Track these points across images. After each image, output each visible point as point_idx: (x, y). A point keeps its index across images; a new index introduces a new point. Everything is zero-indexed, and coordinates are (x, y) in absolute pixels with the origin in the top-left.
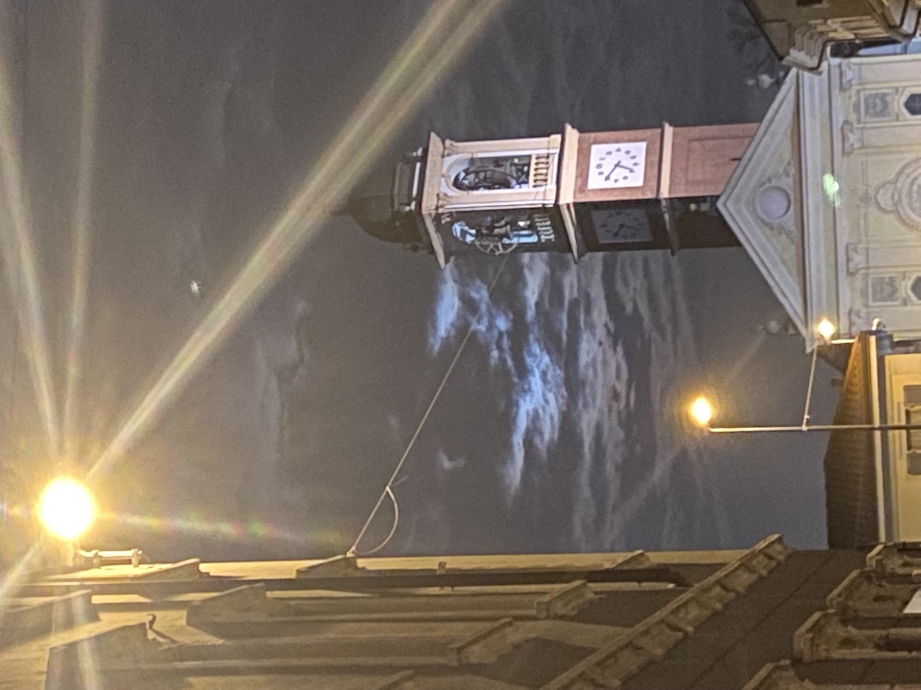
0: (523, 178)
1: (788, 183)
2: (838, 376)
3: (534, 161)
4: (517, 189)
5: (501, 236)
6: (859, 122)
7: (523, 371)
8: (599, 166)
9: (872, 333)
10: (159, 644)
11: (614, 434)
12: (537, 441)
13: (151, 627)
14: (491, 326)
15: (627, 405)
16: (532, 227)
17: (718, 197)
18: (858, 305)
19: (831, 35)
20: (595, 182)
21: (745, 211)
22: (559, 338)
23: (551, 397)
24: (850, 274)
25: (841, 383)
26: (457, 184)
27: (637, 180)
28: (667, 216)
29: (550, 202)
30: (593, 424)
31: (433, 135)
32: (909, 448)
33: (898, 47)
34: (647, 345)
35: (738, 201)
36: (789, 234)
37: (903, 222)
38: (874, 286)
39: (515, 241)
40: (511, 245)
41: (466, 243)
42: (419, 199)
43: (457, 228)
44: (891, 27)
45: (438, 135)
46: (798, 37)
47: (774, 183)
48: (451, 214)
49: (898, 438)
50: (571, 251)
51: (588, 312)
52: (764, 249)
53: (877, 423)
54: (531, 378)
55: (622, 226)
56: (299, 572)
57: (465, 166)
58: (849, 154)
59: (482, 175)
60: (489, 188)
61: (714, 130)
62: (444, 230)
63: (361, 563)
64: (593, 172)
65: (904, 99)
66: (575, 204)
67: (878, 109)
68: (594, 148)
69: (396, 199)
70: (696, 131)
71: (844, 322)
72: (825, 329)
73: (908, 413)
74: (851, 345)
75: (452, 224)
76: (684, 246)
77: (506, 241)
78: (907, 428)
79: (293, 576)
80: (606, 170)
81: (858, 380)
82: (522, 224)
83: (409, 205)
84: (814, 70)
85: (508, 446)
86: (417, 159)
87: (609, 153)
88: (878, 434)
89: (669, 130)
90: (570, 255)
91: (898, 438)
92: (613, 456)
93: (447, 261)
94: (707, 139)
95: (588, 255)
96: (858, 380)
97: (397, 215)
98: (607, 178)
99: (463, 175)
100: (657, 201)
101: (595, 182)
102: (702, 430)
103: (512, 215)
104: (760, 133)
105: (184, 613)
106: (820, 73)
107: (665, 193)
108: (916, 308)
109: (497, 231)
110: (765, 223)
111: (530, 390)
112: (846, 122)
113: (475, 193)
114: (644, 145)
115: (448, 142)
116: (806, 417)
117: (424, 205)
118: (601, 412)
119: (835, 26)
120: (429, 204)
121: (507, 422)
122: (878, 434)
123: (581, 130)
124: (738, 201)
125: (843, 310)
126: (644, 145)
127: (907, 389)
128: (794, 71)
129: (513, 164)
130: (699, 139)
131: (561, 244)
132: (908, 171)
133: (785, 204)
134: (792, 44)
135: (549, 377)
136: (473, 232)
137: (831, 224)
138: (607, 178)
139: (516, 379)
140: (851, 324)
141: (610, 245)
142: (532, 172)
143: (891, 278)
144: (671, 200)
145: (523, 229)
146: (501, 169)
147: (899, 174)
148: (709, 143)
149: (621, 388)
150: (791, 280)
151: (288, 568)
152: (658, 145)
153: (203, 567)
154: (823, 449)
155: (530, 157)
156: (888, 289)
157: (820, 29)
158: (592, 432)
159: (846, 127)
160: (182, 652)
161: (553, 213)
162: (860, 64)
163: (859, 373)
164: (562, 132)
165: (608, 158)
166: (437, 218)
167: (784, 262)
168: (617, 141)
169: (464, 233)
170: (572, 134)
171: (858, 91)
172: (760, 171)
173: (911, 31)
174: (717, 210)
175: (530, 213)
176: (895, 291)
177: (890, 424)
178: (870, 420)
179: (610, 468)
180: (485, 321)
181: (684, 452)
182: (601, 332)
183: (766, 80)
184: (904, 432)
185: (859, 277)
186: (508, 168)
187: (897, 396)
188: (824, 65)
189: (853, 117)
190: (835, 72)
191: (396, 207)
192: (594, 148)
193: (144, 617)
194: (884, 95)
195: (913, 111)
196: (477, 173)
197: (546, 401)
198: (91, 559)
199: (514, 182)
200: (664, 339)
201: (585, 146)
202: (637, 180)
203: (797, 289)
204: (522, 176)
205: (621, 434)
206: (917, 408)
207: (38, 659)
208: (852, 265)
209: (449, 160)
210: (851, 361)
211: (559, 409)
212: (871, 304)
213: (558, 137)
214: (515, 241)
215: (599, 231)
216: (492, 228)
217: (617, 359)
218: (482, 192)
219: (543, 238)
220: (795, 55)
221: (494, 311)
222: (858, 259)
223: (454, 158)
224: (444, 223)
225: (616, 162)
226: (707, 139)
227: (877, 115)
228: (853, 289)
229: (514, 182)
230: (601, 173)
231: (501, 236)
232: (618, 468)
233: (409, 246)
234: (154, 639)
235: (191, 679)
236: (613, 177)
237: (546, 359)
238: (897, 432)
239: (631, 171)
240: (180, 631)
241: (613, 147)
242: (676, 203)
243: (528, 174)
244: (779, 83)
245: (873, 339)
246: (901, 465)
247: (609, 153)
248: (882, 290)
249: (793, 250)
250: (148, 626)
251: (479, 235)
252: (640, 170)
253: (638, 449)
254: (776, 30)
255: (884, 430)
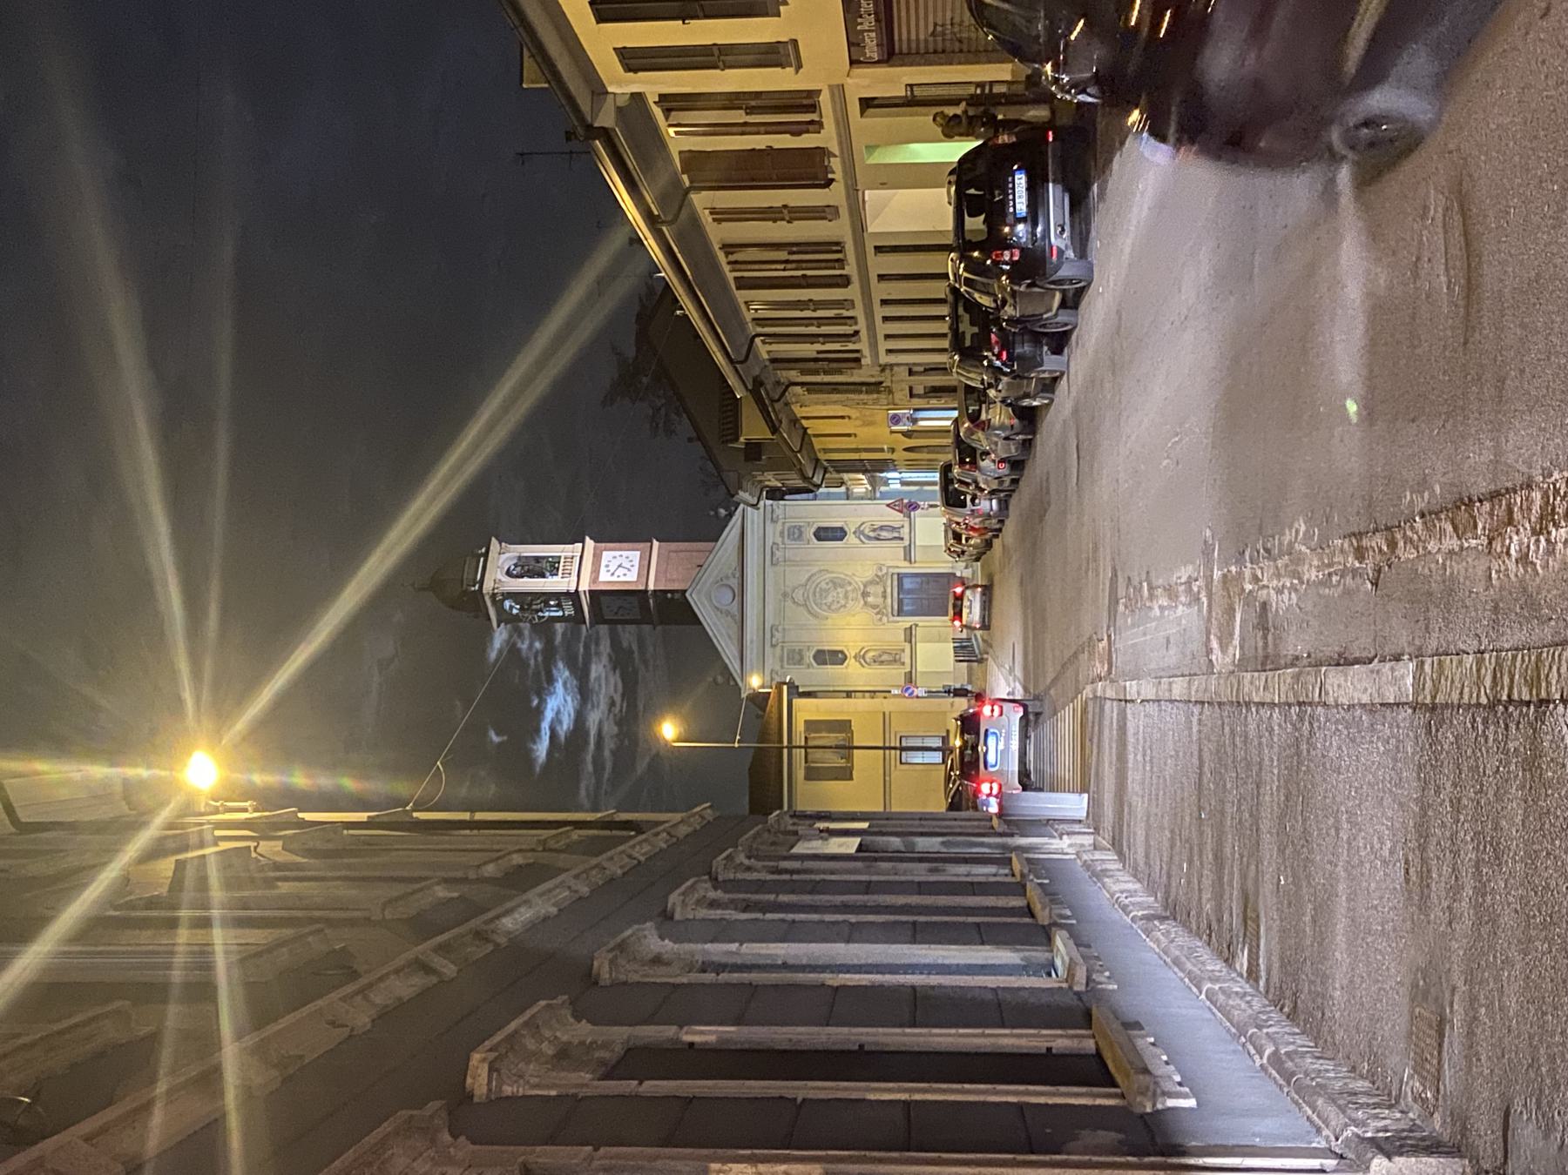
0: (555, 571)
1: (734, 583)
2: (760, 713)
3: (562, 560)
4: (550, 579)
5: (537, 611)
6: (783, 543)
7: (551, 680)
8: (607, 566)
9: (785, 683)
10: (259, 861)
11: (610, 729)
12: (558, 728)
13: (255, 851)
14: (531, 646)
15: (621, 711)
16: (559, 606)
17: (685, 591)
18: (777, 668)
19: (767, 483)
20: (604, 576)
21: (704, 599)
22: (576, 658)
23: (569, 699)
24: (773, 646)
25: (762, 717)
26: (509, 573)
27: (632, 576)
28: (651, 601)
29: (572, 589)
30: (597, 722)
31: (493, 539)
32: (806, 762)
33: (811, 495)
34: (636, 672)
35: (699, 592)
36: (733, 617)
37: (810, 612)
38: (788, 655)
39: (547, 614)
40: (544, 617)
41: (511, 614)
42: (482, 582)
43: (507, 604)
44: (805, 478)
45: (497, 539)
46: (744, 484)
47: (725, 582)
48: (503, 594)
49: (799, 754)
50: (585, 623)
51: (597, 644)
52: (715, 624)
53: (785, 743)
54: (556, 684)
55: (620, 608)
56: (369, 817)
57: (515, 561)
58: (776, 565)
59: (526, 568)
60: (530, 577)
61: (686, 545)
62: (498, 605)
63: (415, 815)
64: (603, 569)
65: (813, 530)
66: (590, 591)
67: (796, 536)
68: (605, 553)
69: (465, 582)
70: (673, 546)
71: (768, 678)
72: (755, 682)
73: (806, 738)
74: (769, 693)
75: (503, 600)
76: (661, 623)
77: (540, 614)
78: (806, 748)
79: (365, 820)
80: (612, 569)
81: (775, 716)
82: (552, 603)
83: (474, 586)
84: (755, 506)
85: (538, 730)
86: (482, 555)
87: (615, 557)
88: (785, 751)
89: (656, 543)
90: (584, 627)
91: (799, 754)
92: (610, 745)
93: (499, 626)
94: (681, 551)
95: (597, 626)
96: (775, 716)
97: (465, 593)
98: (613, 574)
99: (513, 567)
100: (646, 591)
101: (604, 576)
102: (666, 741)
103: (546, 597)
104: (717, 548)
105: (280, 843)
106: (758, 509)
107: (651, 587)
108: (815, 671)
109: (534, 607)
110: (718, 609)
111: (555, 692)
112: (774, 543)
113: (521, 580)
114: (639, 553)
115: (503, 544)
116: (738, 737)
117: (484, 587)
118: (603, 713)
119: (770, 477)
120: (488, 586)
121: (539, 712)
122: (785, 751)
123: (596, 541)
124: (699, 592)
125: (767, 672)
126: (639, 553)
127: (806, 722)
128: (742, 506)
129: (548, 562)
130: (676, 552)
131: (578, 618)
132: (813, 579)
133: (731, 595)
134: (740, 488)
135: (569, 686)
136: (518, 607)
137: (762, 595)
138: (613, 574)
139: (546, 686)
140: (772, 679)
141: (611, 620)
142: (561, 568)
143: (800, 650)
144: (655, 591)
145: (553, 606)
146: (540, 565)
147: (808, 580)
148: (682, 555)
149: (618, 699)
150: (733, 648)
151: (362, 816)
152: (648, 554)
153: (300, 815)
154: (749, 760)
155: (560, 557)
156: (797, 657)
157: (759, 478)
158: (596, 727)
159: (775, 546)
160: (277, 867)
161: (574, 596)
162: (785, 505)
163: (775, 710)
164: (583, 542)
165: (613, 561)
166: (494, 596)
167: (729, 637)
168: (621, 550)
169: (511, 607)
170: (589, 542)
171: (784, 523)
172: (716, 572)
173: (819, 483)
174: (686, 598)
175: (557, 596)
176: (802, 658)
177: (794, 744)
178: (781, 741)
179: (607, 753)
180: (527, 642)
181: (657, 755)
182: (605, 660)
183: (722, 512)
184: (803, 750)
185: (779, 648)
186: (544, 564)
187: (800, 727)
188: (762, 503)
189: (779, 540)
190: (769, 509)
191: (465, 586)
192: (605, 553)
193: (252, 844)
194: (800, 527)
195: (819, 539)
196: (523, 567)
197: (565, 701)
198: (217, 807)
199: (548, 574)
200: (647, 671)
201: (598, 552)
202: (632, 576)
203: (737, 654)
204: (554, 570)
205: (615, 730)
206: (812, 735)
207: (166, 869)
208: (774, 640)
209: (503, 557)
210: (770, 702)
211: (574, 707)
212: (786, 666)
213: (580, 545)
214: (547, 614)
215: (605, 609)
216: (530, 605)
217: (615, 679)
218: (526, 579)
219: (567, 613)
220: (743, 495)
221: (533, 635)
222: (778, 635)
223: (507, 555)
224: (497, 602)
225: (618, 563)
226: (681, 551)
227: (795, 540)
228: (774, 656)
229: (548, 574)
230: (608, 571)
231: (537, 611)
232: (613, 753)
233: (472, 614)
234: (256, 858)
235: (280, 884)
236: (616, 574)
237: (567, 673)
238: (798, 750)
239: (629, 570)
240: (278, 853)
241: (617, 553)
242: (658, 594)
243: (558, 569)
244: (730, 515)
245: (785, 687)
246: (800, 773)
247: (615, 557)
248: (793, 658)
249: (735, 628)
250: (252, 849)
251: (521, 609)
252: (635, 570)
253: (626, 742)
254: (731, 477)
255: (790, 748)
